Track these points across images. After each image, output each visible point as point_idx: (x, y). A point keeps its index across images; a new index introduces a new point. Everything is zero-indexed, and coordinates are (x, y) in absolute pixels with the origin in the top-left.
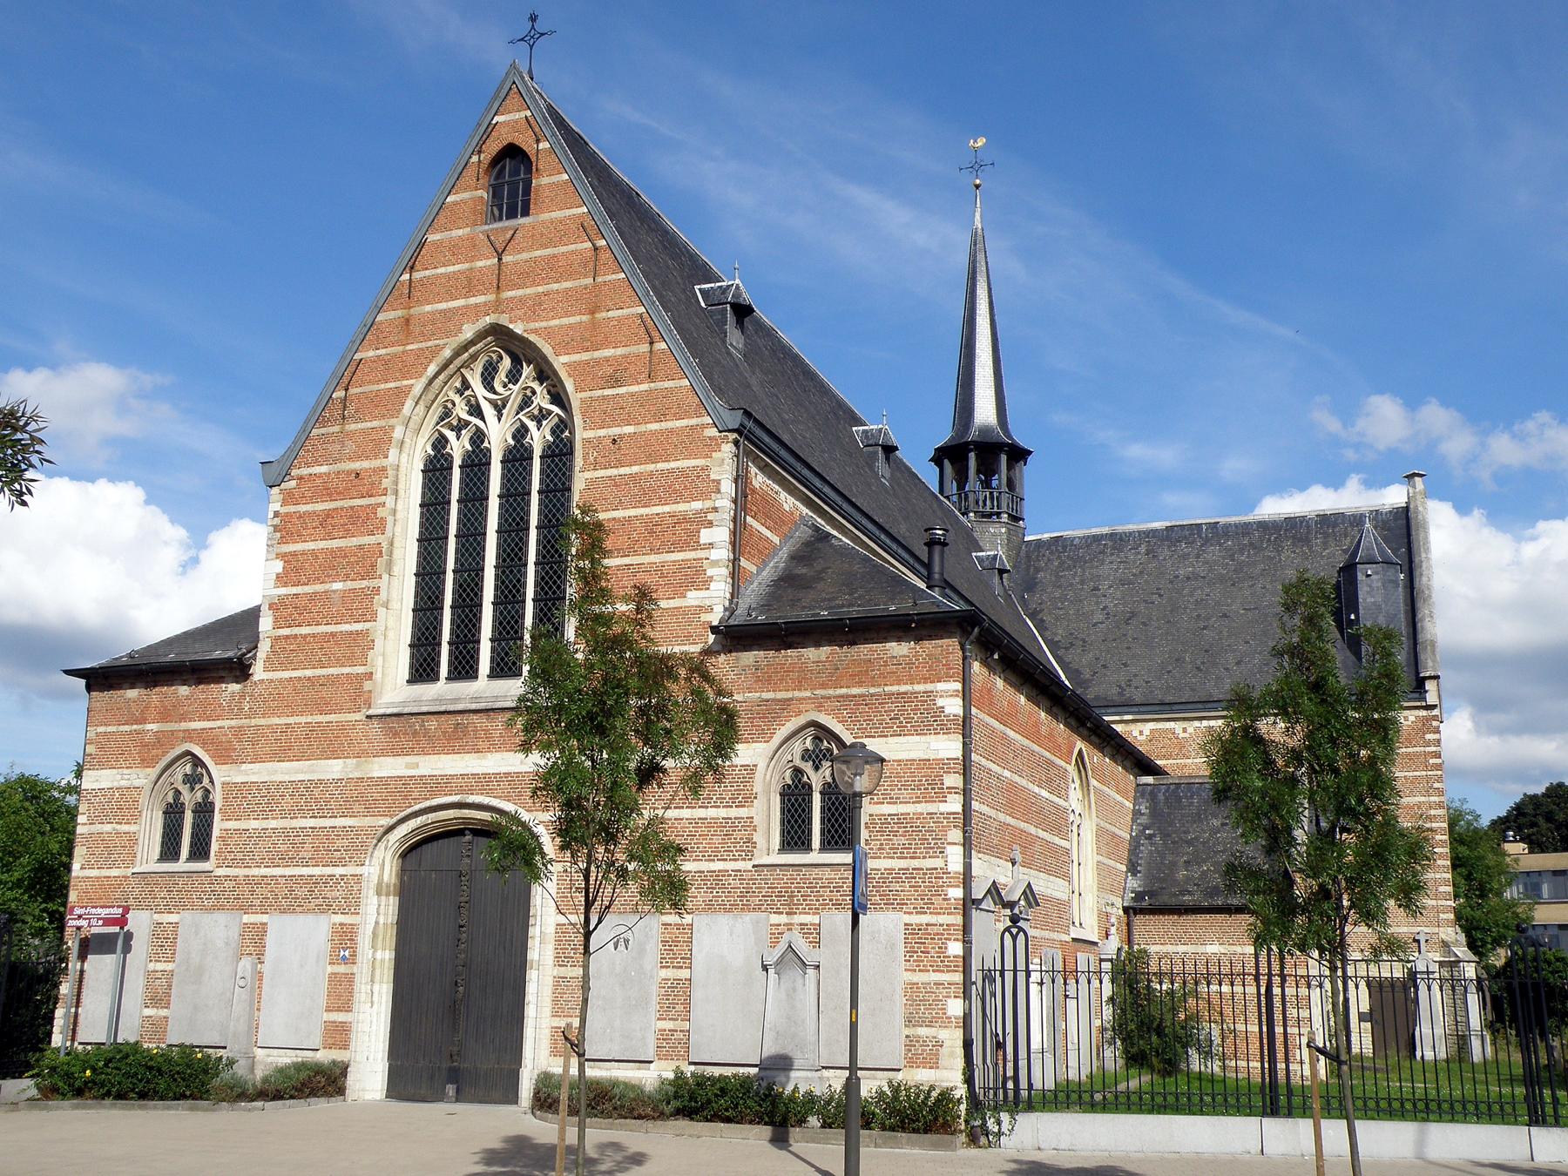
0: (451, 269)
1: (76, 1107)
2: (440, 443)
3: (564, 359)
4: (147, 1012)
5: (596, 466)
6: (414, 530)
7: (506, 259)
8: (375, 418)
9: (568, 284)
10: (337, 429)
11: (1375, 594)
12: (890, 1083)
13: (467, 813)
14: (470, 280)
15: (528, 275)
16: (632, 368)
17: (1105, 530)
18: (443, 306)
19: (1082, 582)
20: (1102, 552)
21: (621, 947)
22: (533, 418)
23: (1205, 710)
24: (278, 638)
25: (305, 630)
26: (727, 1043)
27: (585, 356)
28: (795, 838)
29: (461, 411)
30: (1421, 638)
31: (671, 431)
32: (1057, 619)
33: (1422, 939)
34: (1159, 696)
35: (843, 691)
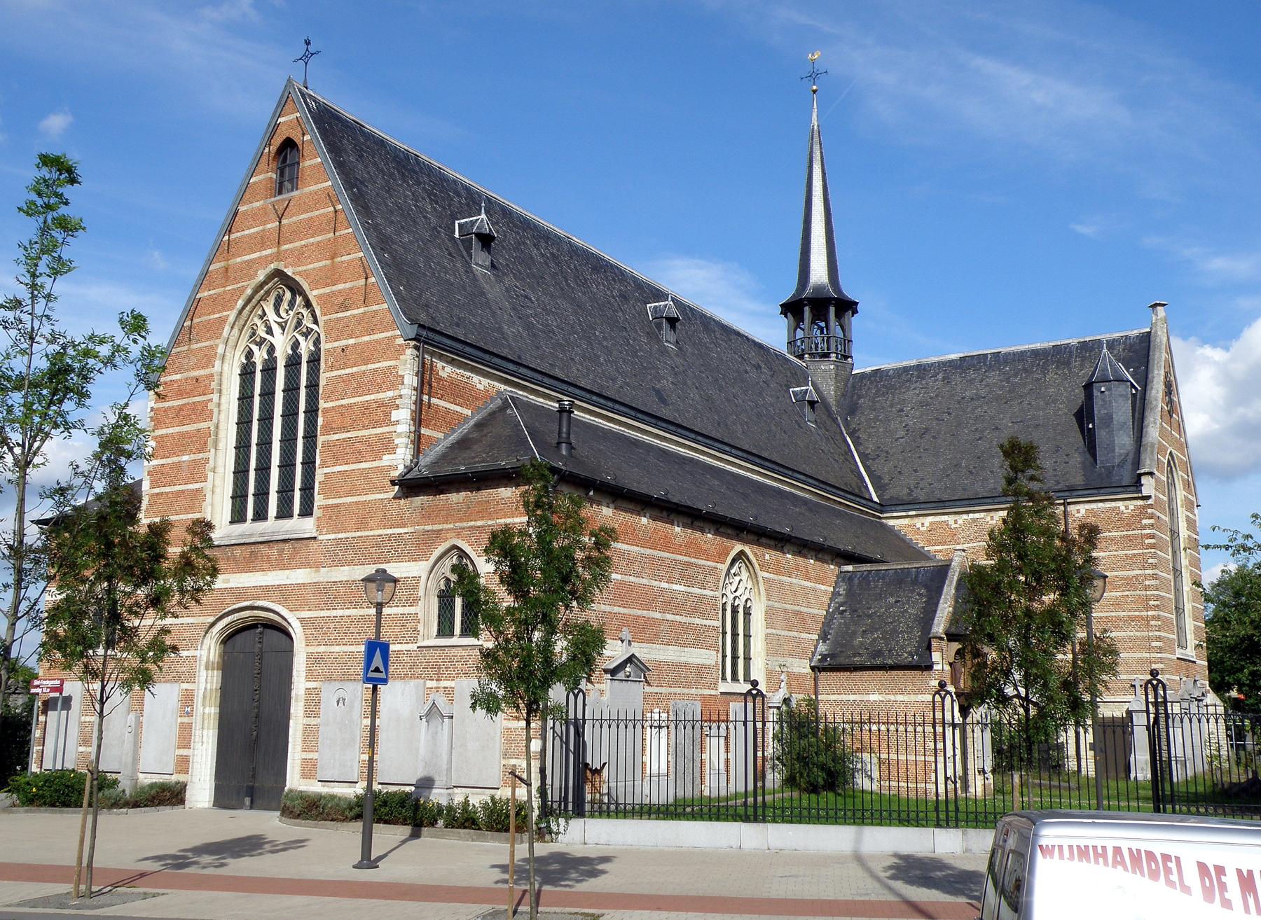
0: (252, 231)
1: (26, 812)
2: (250, 354)
3: (315, 292)
4: (81, 749)
5: (332, 368)
6: (234, 417)
7: (284, 221)
8: (208, 339)
9: (319, 238)
10: (186, 348)
11: (1115, 405)
12: (493, 798)
13: (256, 613)
14: (262, 238)
15: (296, 233)
16: (355, 297)
17: (913, 362)
18: (247, 258)
19: (891, 406)
20: (909, 381)
21: (341, 704)
22: (303, 334)
23: (970, 505)
24: (152, 495)
25: (167, 489)
26: (397, 772)
27: (327, 290)
28: (445, 629)
29: (262, 332)
30: (1145, 441)
31: (376, 341)
32: (869, 436)
33: (1137, 684)
34: (938, 495)
35: (472, 523)
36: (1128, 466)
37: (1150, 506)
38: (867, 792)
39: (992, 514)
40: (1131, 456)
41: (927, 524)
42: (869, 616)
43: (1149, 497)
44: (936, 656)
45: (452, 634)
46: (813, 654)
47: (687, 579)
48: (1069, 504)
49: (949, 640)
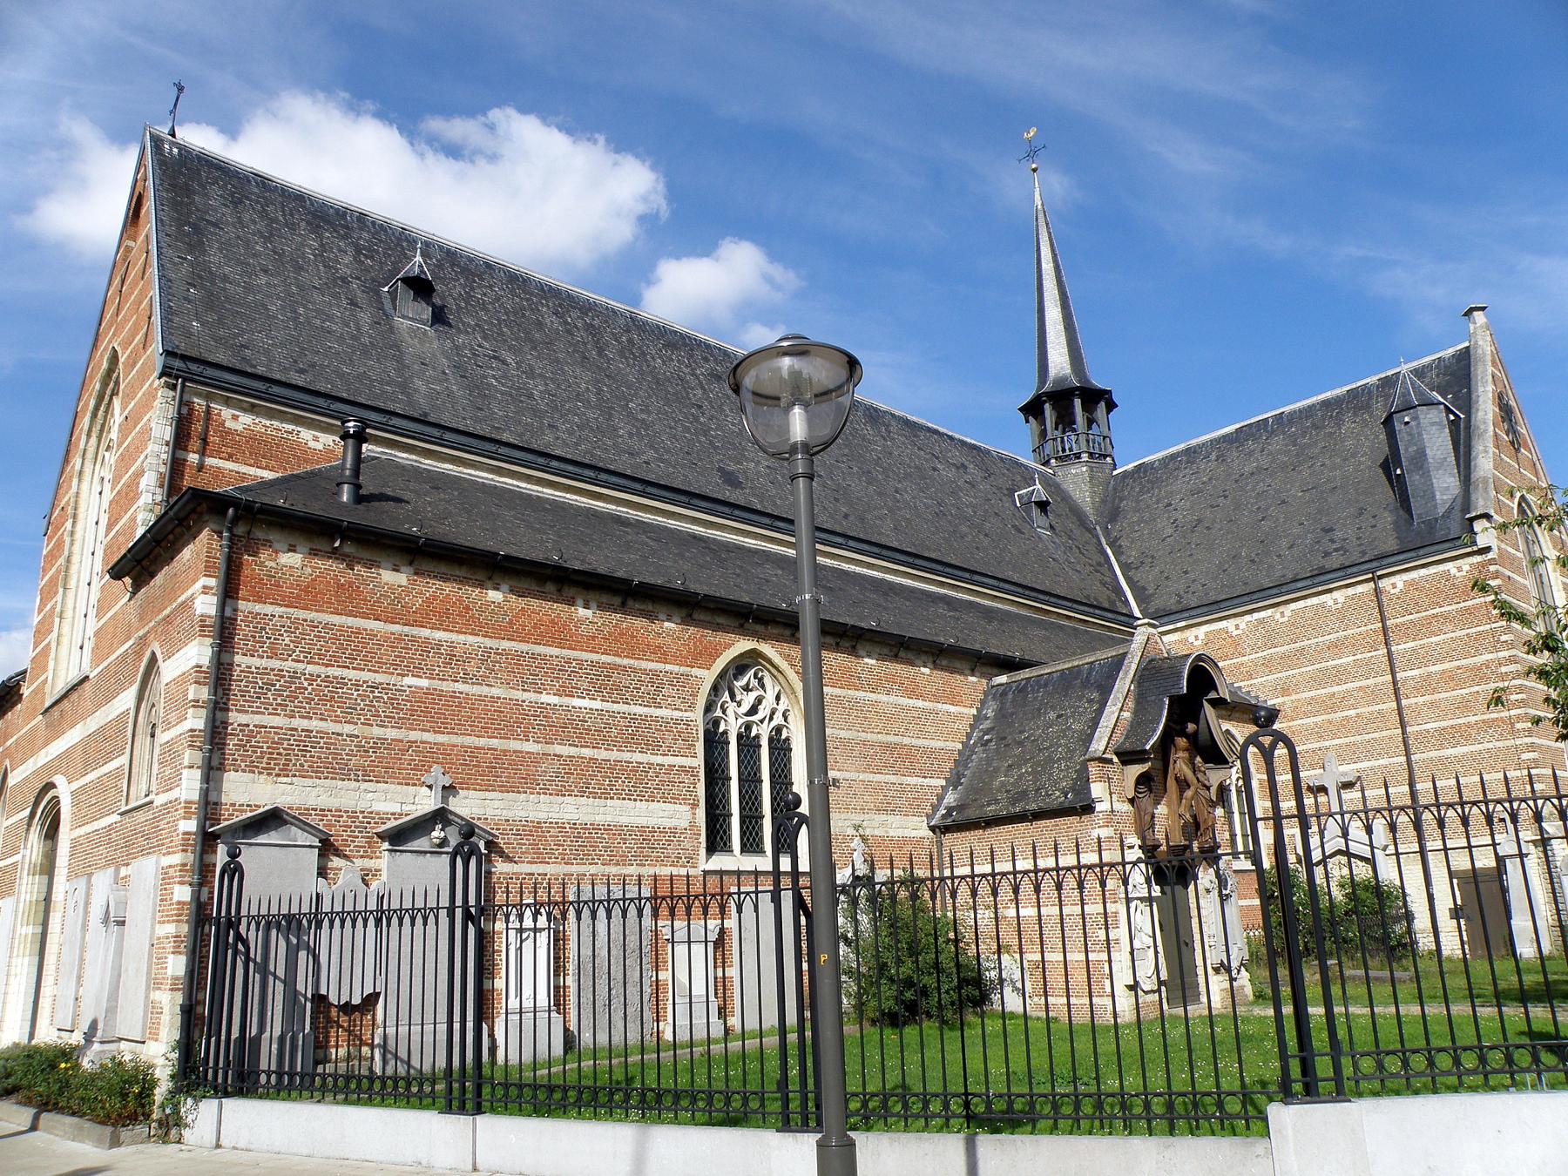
30: (1474, 477)
36: (1456, 514)
37: (1492, 562)
38: (1013, 1015)
39: (1282, 609)
40: (1459, 501)
41: (1202, 636)
42: (1020, 744)
43: (1487, 549)
44: (1097, 790)
45: (727, 848)
46: (935, 808)
47: (616, 692)
48: (1380, 577)
49: (1124, 763)
